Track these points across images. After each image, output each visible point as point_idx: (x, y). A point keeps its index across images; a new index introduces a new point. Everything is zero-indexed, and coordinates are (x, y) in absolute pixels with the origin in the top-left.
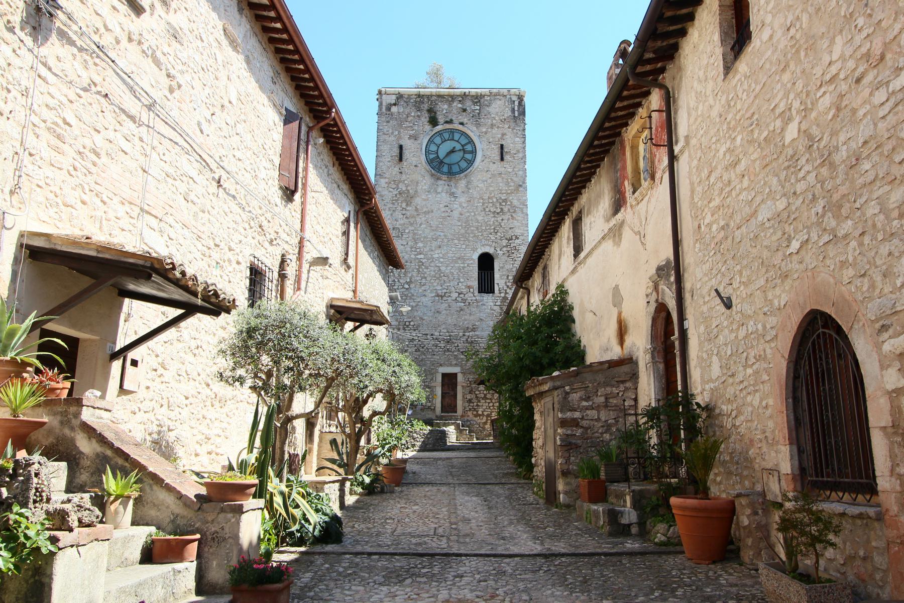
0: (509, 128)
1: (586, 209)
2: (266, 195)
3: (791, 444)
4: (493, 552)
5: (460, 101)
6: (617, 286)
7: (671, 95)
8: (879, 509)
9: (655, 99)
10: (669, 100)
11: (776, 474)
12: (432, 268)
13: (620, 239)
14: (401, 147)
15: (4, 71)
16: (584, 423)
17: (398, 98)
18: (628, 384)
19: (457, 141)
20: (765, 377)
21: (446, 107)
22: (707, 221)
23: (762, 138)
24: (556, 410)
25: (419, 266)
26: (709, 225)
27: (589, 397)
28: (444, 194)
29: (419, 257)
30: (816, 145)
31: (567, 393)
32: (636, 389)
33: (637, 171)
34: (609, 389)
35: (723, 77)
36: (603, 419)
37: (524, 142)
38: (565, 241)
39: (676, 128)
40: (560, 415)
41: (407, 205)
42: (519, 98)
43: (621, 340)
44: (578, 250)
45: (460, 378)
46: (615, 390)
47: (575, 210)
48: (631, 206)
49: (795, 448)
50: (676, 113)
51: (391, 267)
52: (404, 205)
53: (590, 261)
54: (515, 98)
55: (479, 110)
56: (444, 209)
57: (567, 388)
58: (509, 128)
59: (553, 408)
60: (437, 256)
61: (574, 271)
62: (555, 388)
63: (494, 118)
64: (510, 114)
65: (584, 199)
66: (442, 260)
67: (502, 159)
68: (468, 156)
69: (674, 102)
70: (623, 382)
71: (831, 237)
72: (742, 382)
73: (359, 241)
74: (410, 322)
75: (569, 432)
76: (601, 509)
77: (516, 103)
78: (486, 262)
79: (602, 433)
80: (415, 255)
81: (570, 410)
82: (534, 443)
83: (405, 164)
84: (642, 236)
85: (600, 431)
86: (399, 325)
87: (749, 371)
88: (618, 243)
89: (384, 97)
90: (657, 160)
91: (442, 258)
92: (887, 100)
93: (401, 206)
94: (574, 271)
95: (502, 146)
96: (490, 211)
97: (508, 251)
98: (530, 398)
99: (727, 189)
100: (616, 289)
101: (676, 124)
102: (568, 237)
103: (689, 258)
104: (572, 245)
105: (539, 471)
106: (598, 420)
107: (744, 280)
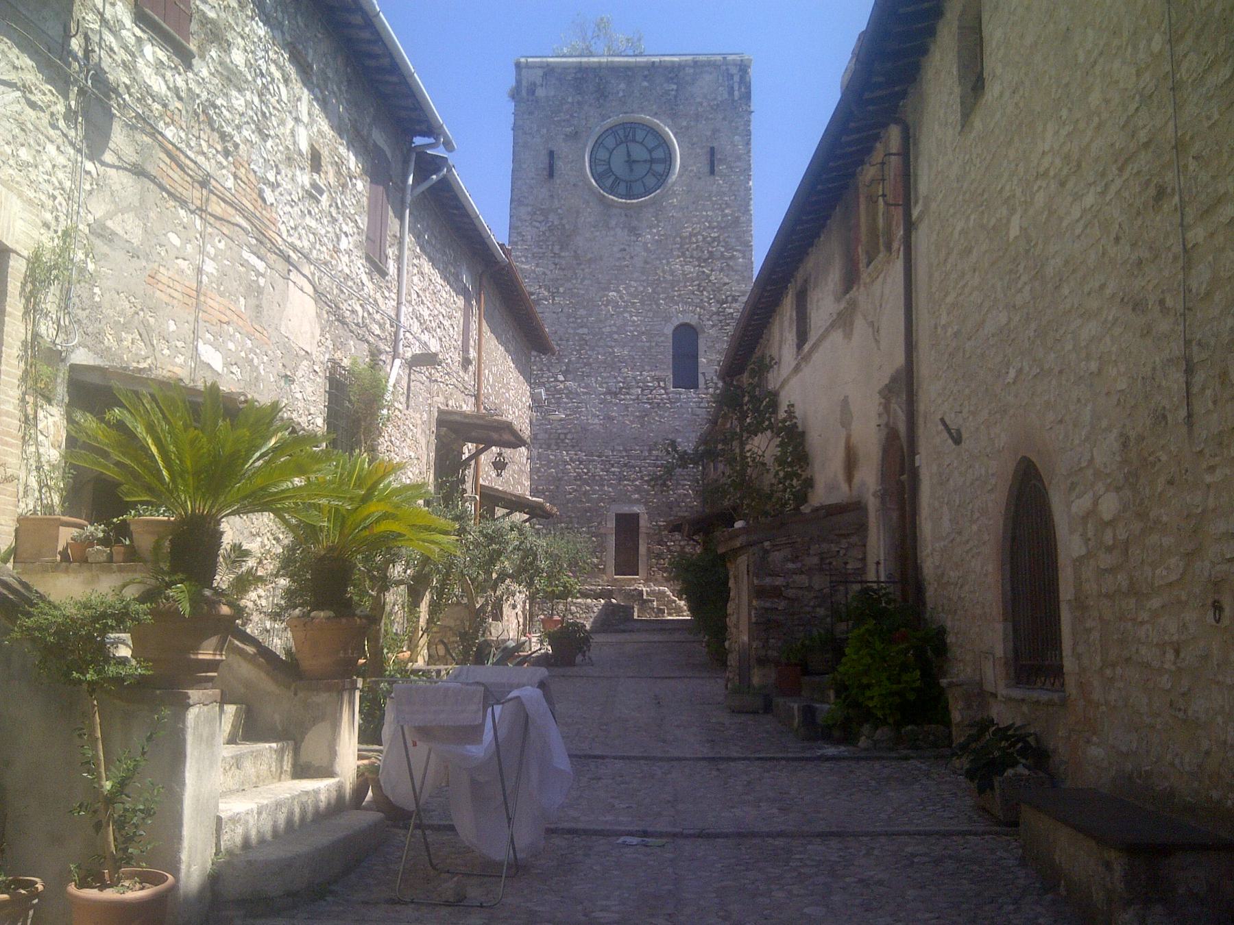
0: (724, 119)
1: (812, 280)
2: (348, 273)
3: (1005, 620)
4: (645, 755)
5: (646, 77)
6: (846, 397)
7: (911, 134)
8: (1062, 694)
9: (894, 133)
10: (909, 139)
11: (991, 656)
12: (601, 350)
13: (852, 330)
14: (551, 154)
15: (50, 176)
16: (791, 593)
17: (545, 74)
18: (854, 539)
19: (641, 143)
20: (986, 537)
21: (622, 86)
22: (943, 322)
23: (992, 223)
24: (751, 574)
25: (580, 345)
26: (944, 327)
27: (797, 557)
28: (619, 231)
29: (580, 331)
30: (1032, 250)
31: (766, 552)
32: (865, 546)
33: (873, 230)
34: (825, 546)
35: (960, 128)
36: (816, 587)
37: (748, 143)
38: (786, 324)
39: (916, 181)
40: (756, 582)
41: (561, 249)
42: (740, 70)
43: (849, 478)
44: (802, 337)
45: (644, 522)
46: (834, 548)
47: (800, 275)
48: (865, 284)
49: (1010, 625)
50: (916, 158)
51: (534, 353)
52: (557, 248)
53: (816, 357)
54: (734, 70)
55: (677, 90)
56: (619, 255)
57: (767, 544)
58: (724, 119)
59: (748, 571)
60: (608, 329)
61: (797, 369)
62: (751, 544)
63: (701, 104)
64: (726, 96)
65: (810, 263)
66: (616, 336)
67: (712, 172)
68: (659, 168)
69: (915, 144)
70: (846, 536)
71: (1038, 371)
72: (967, 542)
73: (484, 323)
74: (566, 434)
75: (768, 605)
76: (796, 706)
77: (736, 78)
78: (686, 338)
79: (814, 607)
80: (575, 329)
81: (770, 575)
82: (728, 619)
83: (558, 181)
84: (876, 330)
85: (812, 604)
86: (549, 439)
87: (975, 528)
88: (848, 335)
89: (524, 71)
90: (894, 223)
91: (616, 333)
92: (1081, 217)
93: (552, 250)
94: (797, 369)
95: (712, 151)
96: (692, 257)
97: (721, 321)
98: (723, 556)
99: (961, 284)
100: (845, 402)
101: (916, 175)
102: (791, 318)
103: (924, 369)
104: (795, 330)
105: (732, 659)
106: (810, 588)
107: (972, 408)
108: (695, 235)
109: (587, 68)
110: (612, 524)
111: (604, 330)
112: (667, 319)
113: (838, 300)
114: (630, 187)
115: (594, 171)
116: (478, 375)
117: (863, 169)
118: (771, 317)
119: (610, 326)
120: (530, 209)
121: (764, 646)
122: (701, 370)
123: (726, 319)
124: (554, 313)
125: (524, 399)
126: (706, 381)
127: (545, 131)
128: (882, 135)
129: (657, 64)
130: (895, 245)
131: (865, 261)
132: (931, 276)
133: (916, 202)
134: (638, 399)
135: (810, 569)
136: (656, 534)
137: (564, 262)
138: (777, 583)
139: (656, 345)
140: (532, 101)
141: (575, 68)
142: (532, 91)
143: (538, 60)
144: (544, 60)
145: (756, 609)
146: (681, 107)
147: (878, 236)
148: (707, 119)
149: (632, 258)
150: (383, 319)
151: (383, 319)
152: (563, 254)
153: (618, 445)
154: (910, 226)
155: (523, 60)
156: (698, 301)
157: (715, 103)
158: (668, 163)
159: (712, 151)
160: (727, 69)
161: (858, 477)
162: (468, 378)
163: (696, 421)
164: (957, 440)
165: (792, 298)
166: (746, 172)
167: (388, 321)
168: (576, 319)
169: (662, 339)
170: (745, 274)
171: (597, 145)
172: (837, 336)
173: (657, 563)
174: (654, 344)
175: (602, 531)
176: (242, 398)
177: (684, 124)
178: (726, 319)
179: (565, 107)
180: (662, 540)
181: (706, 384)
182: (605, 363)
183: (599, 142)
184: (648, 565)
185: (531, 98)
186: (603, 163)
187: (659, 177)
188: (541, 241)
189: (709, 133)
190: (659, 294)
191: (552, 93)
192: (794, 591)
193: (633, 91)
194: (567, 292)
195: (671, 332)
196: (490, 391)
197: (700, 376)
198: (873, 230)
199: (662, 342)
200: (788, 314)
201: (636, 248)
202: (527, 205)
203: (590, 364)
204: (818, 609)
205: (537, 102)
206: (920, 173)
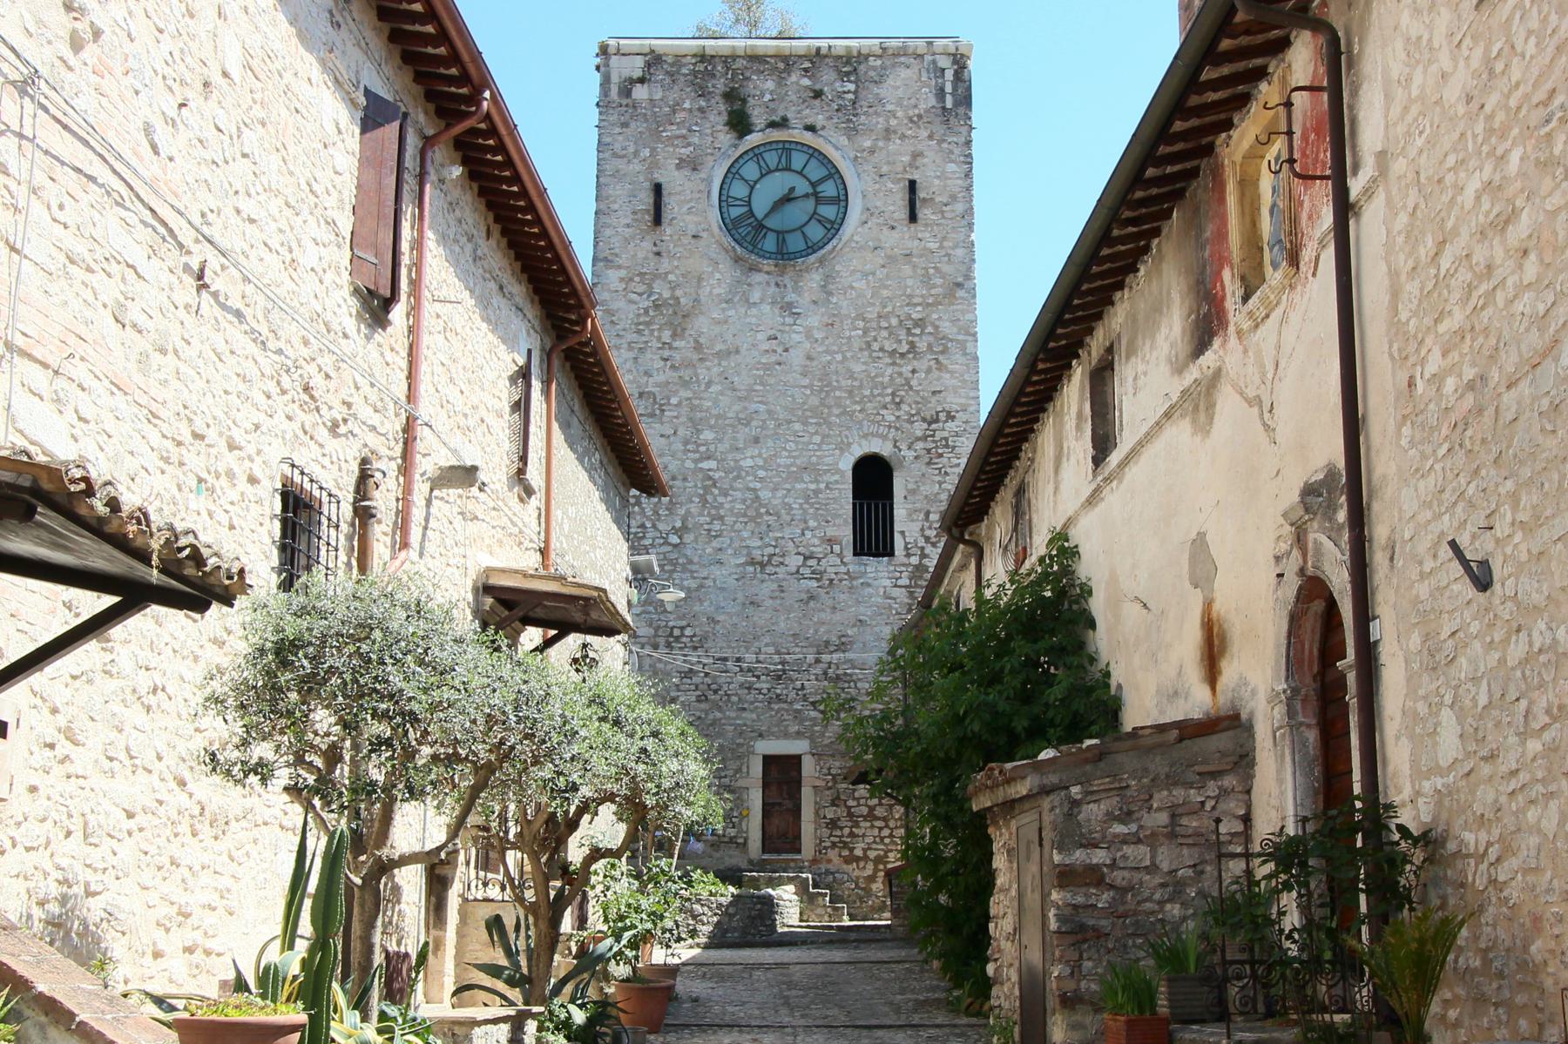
0: (930, 137)
1: (1124, 342)
5: (806, 70)
6: (1201, 536)
12: (738, 494)
14: (658, 189)
16: (1119, 877)
17: (649, 65)
18: (1229, 781)
19: (800, 173)
21: (770, 85)
22: (1431, 369)
26: (1437, 380)
27: (1129, 813)
28: (766, 308)
29: (705, 465)
31: (1075, 803)
32: (1248, 792)
33: (1253, 243)
34: (1180, 794)
37: (968, 175)
38: (1070, 422)
40: (1057, 858)
41: (674, 336)
42: (955, 62)
43: (1212, 673)
45: (808, 767)
46: (1195, 796)
47: (1096, 344)
48: (1239, 333)
50: (1355, 93)
51: (634, 492)
52: (666, 335)
53: (1134, 472)
55: (855, 92)
56: (766, 346)
58: (930, 137)
61: (1093, 500)
62: (1045, 791)
64: (932, 101)
65: (1118, 316)
67: (913, 218)
69: (1350, 66)
70: (1215, 775)
73: (555, 426)
74: (682, 628)
75: (1080, 899)
77: (949, 75)
79: (1161, 903)
80: (696, 461)
83: (668, 231)
84: (1266, 408)
85: (1157, 896)
89: (614, 60)
90: (1304, 216)
91: (761, 468)
93: (659, 339)
94: (1093, 500)
95: (912, 185)
97: (929, 451)
99: (1484, 288)
101: (1354, 121)
102: (1080, 415)
103: (1383, 462)
104: (1089, 433)
106: (1153, 869)
108: (886, 317)
109: (713, 56)
110: (757, 768)
111: (742, 463)
112: (843, 447)
113: (1179, 370)
114: (784, 240)
115: (726, 215)
116: (546, 516)
117: (1230, 137)
118: (1037, 420)
119: (752, 457)
120: (623, 273)
121: (1072, 973)
122: (897, 527)
123: (937, 447)
124: (662, 436)
125: (618, 566)
126: (906, 544)
127: (647, 152)
128: (1270, 70)
129: (824, 51)
130: (1307, 255)
131: (1240, 293)
132: (1395, 294)
133: (1356, 168)
134: (798, 572)
135: (1153, 834)
136: (830, 788)
137: (678, 357)
138: (1095, 861)
139: (827, 487)
140: (627, 106)
141: (694, 56)
142: (626, 91)
143: (637, 42)
144: (647, 42)
145: (1058, 908)
146: (863, 117)
147: (1261, 249)
148: (903, 137)
149: (786, 350)
150: (382, 400)
151: (382, 400)
152: (676, 344)
153: (767, 645)
154: (1344, 209)
155: (612, 42)
156: (893, 418)
157: (917, 112)
158: (843, 204)
159: (912, 185)
160: (934, 62)
161: (1230, 671)
162: (529, 513)
163: (890, 607)
164: (1482, 579)
165: (1082, 382)
166: (967, 218)
167: (392, 405)
168: (699, 446)
169: (836, 477)
170: (966, 377)
171: (730, 176)
172: (1180, 432)
173: (831, 835)
174: (822, 486)
175: (741, 783)
176: (78, 474)
177: (868, 144)
178: (937, 447)
179: (680, 116)
180: (838, 798)
181: (906, 548)
182: (745, 515)
183: (734, 170)
184: (816, 837)
185: (624, 102)
186: (762, 163)
187: (829, 226)
188: (640, 324)
189: (906, 159)
190: (829, 407)
191: (658, 95)
192: (1126, 874)
193: (786, 94)
194: (685, 403)
195: (851, 467)
196: (565, 545)
197: (897, 537)
198: (1253, 243)
199: (837, 482)
200: (1074, 409)
201: (794, 336)
202: (619, 267)
203: (721, 518)
204: (1168, 907)
205: (634, 107)
206: (1361, 115)
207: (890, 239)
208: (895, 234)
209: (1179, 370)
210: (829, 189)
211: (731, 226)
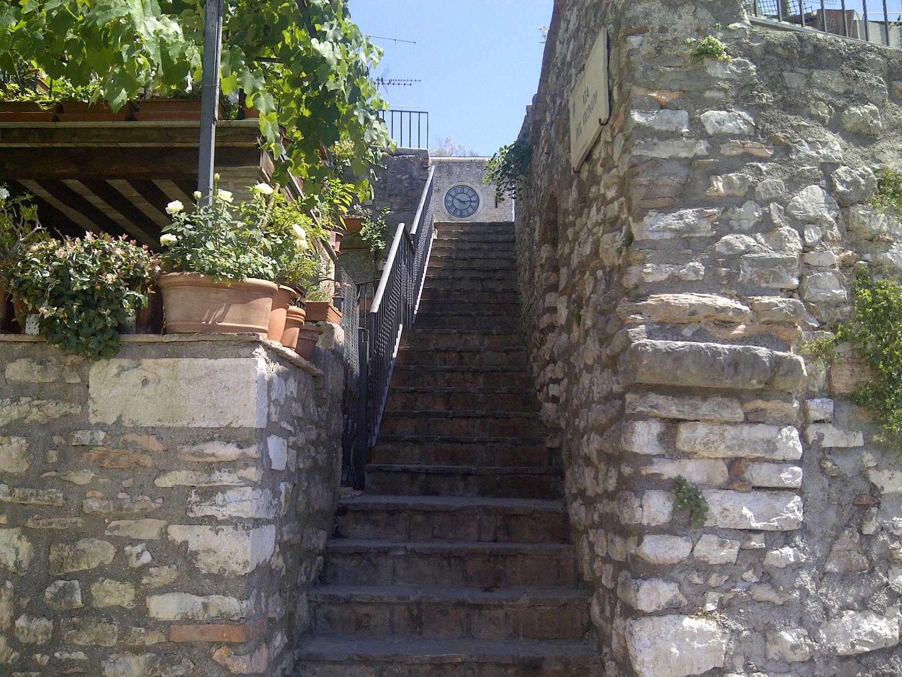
21: (458, 170)
65: (760, 22)
67: (496, 207)
207: (490, 212)
208: (492, 211)
209: (222, 96)
210: (474, 199)
211: (448, 208)
